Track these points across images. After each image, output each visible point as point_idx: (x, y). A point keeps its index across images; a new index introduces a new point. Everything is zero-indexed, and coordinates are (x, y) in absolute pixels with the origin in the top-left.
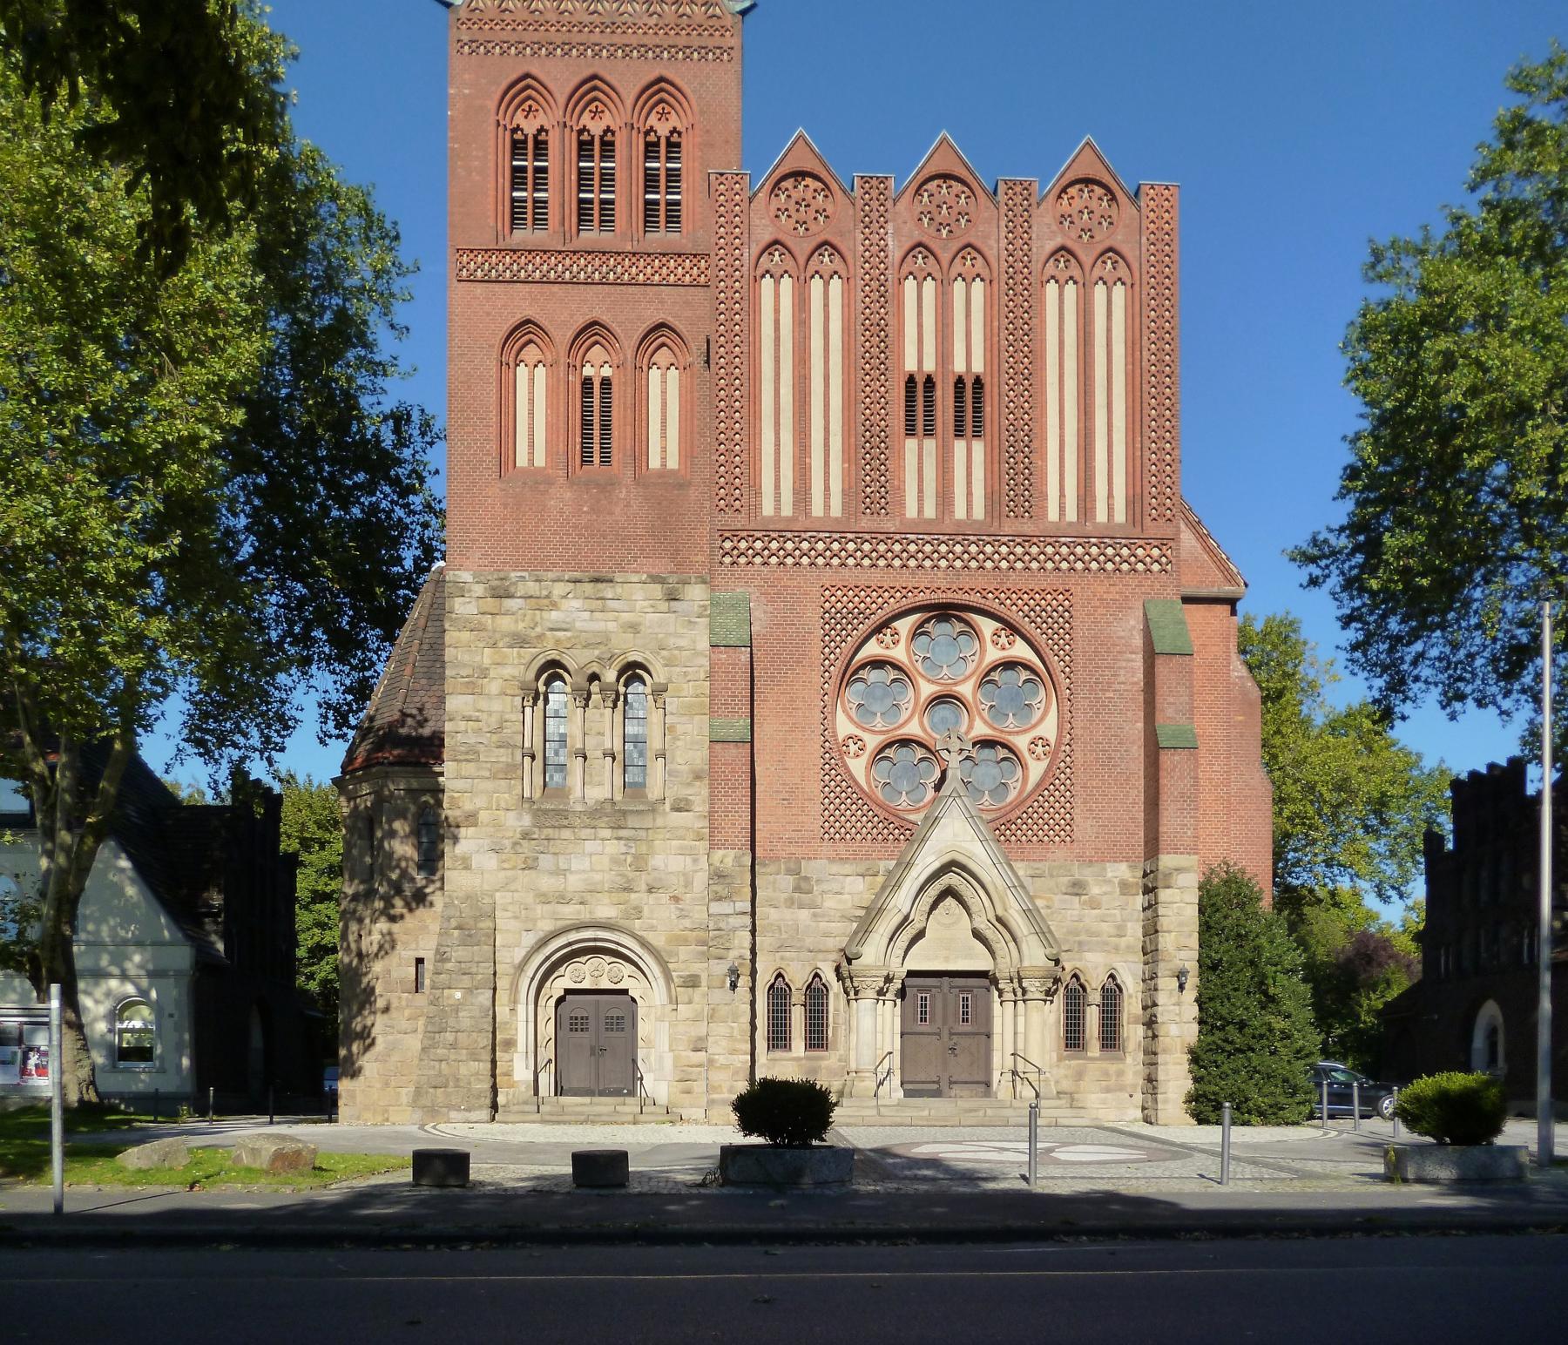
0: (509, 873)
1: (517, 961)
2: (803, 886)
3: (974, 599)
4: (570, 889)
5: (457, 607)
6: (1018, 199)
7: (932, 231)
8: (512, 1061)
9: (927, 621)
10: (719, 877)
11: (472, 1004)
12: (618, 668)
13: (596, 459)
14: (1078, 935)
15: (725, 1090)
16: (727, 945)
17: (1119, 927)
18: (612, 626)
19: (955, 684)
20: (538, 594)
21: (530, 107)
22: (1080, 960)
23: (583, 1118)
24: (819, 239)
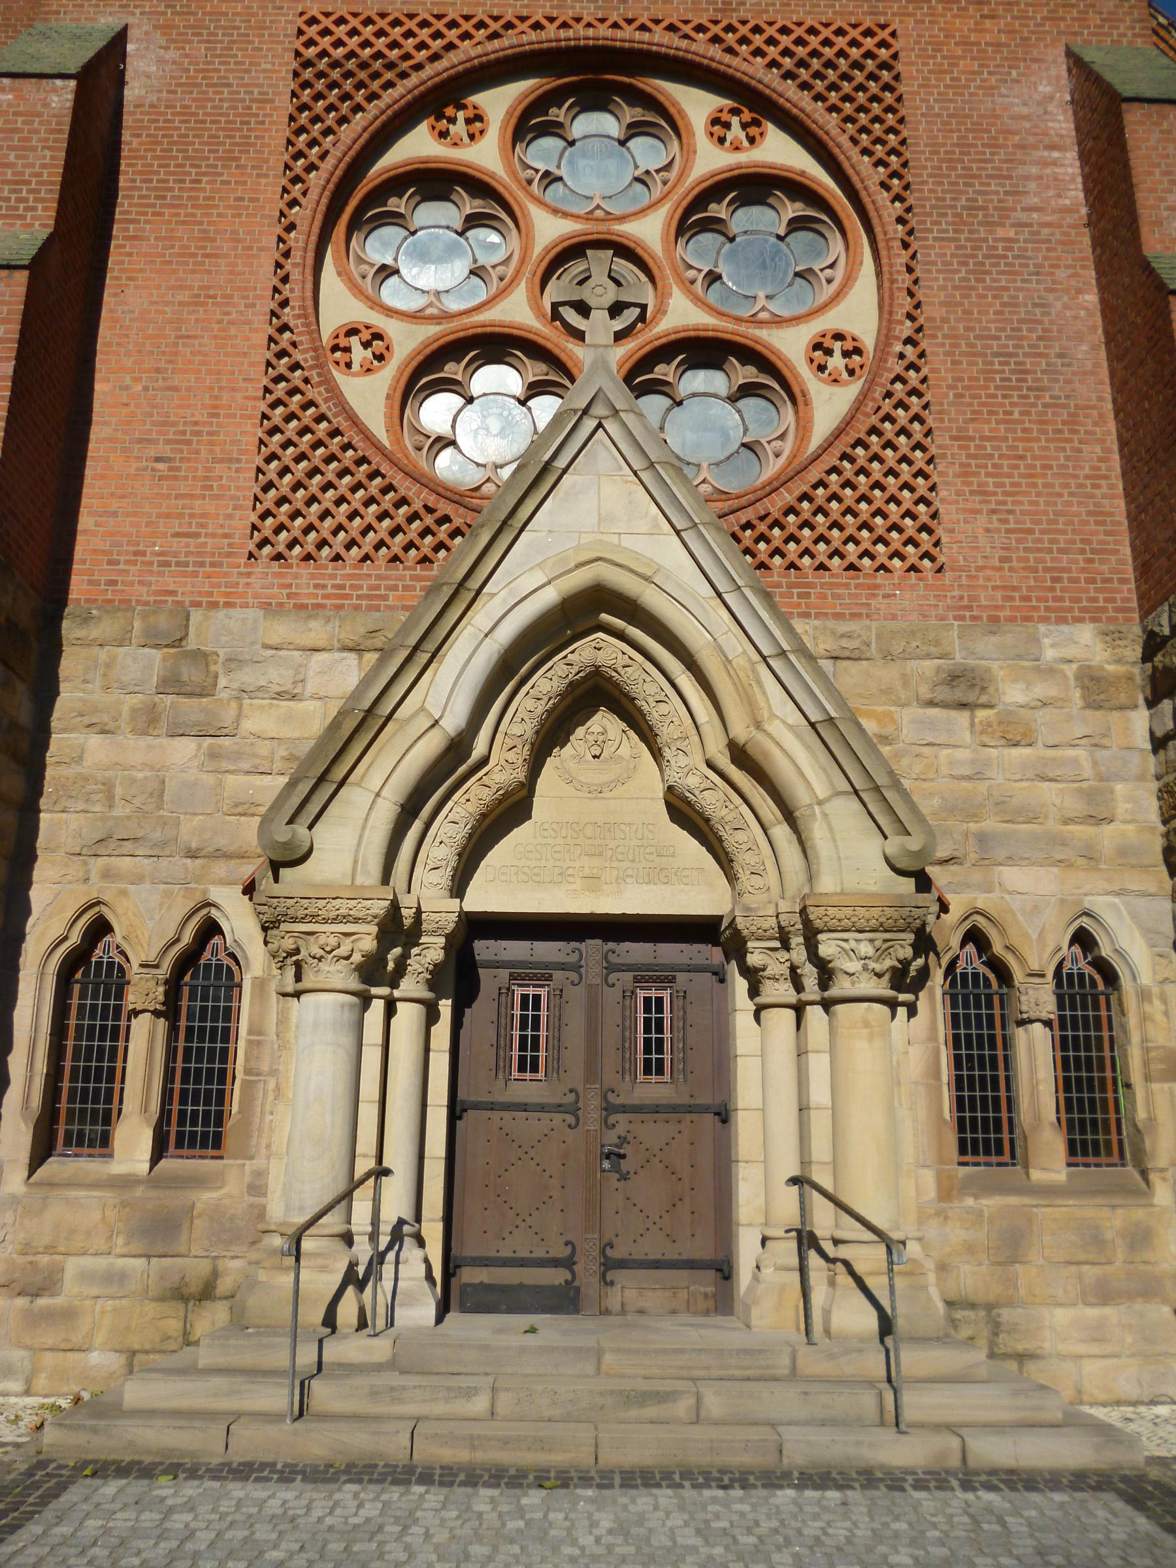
14: (975, 817)
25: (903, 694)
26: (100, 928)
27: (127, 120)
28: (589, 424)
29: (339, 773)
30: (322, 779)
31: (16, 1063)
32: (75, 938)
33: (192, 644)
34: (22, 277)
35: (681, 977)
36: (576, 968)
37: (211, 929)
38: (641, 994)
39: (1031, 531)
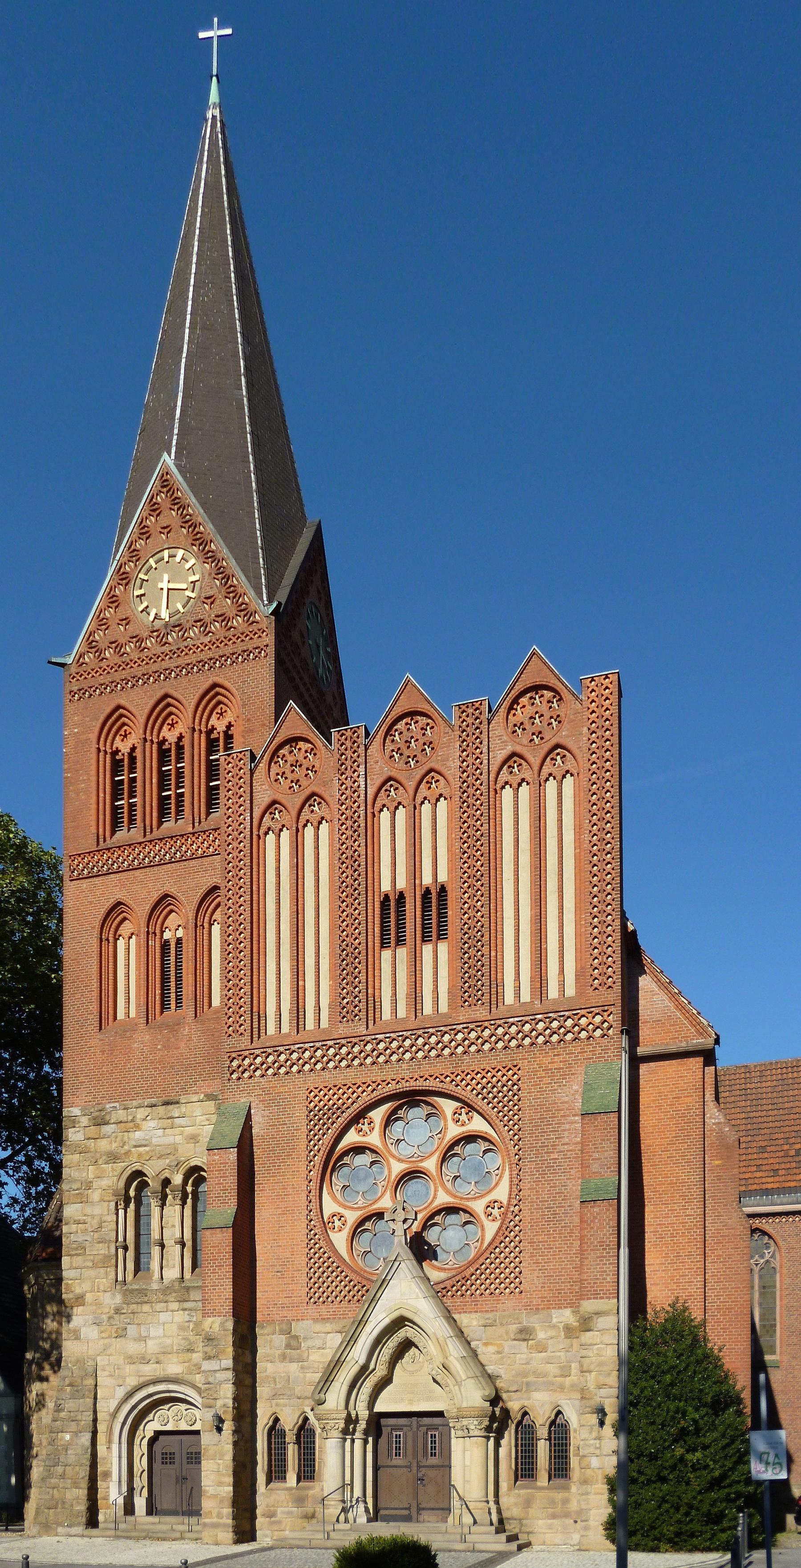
0: (106, 1341)
1: (112, 1410)
2: (293, 1342)
3: (432, 1084)
4: (149, 1351)
5: (70, 1135)
6: (470, 720)
7: (402, 765)
8: (108, 1488)
9: (400, 1107)
10: (209, 1340)
11: (77, 1444)
12: (183, 1172)
13: (173, 1006)
14: (525, 1377)
15: (214, 1515)
16: (215, 1396)
17: (562, 1368)
18: (178, 1139)
19: (421, 1161)
20: (125, 1119)
21: (125, 731)
22: (529, 1399)
23: (144, 1534)
24: (307, 792)
25: (506, 1337)
26: (277, 1420)
27: (255, 1143)
28: (397, 1264)
29: (331, 1378)
30: (326, 1381)
31: (259, 1458)
32: (271, 1423)
33: (293, 1333)
34: (231, 1230)
35: (440, 1428)
36: (410, 1426)
37: (306, 1419)
38: (430, 1433)
39: (552, 1276)
